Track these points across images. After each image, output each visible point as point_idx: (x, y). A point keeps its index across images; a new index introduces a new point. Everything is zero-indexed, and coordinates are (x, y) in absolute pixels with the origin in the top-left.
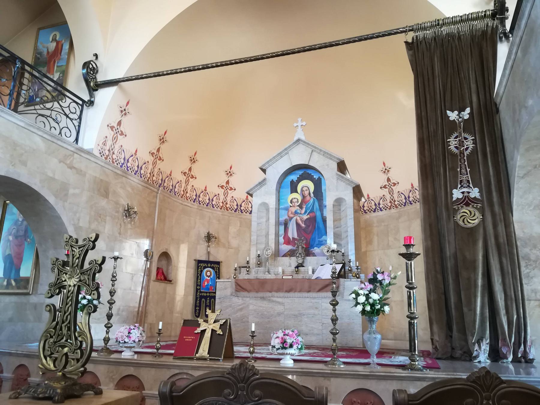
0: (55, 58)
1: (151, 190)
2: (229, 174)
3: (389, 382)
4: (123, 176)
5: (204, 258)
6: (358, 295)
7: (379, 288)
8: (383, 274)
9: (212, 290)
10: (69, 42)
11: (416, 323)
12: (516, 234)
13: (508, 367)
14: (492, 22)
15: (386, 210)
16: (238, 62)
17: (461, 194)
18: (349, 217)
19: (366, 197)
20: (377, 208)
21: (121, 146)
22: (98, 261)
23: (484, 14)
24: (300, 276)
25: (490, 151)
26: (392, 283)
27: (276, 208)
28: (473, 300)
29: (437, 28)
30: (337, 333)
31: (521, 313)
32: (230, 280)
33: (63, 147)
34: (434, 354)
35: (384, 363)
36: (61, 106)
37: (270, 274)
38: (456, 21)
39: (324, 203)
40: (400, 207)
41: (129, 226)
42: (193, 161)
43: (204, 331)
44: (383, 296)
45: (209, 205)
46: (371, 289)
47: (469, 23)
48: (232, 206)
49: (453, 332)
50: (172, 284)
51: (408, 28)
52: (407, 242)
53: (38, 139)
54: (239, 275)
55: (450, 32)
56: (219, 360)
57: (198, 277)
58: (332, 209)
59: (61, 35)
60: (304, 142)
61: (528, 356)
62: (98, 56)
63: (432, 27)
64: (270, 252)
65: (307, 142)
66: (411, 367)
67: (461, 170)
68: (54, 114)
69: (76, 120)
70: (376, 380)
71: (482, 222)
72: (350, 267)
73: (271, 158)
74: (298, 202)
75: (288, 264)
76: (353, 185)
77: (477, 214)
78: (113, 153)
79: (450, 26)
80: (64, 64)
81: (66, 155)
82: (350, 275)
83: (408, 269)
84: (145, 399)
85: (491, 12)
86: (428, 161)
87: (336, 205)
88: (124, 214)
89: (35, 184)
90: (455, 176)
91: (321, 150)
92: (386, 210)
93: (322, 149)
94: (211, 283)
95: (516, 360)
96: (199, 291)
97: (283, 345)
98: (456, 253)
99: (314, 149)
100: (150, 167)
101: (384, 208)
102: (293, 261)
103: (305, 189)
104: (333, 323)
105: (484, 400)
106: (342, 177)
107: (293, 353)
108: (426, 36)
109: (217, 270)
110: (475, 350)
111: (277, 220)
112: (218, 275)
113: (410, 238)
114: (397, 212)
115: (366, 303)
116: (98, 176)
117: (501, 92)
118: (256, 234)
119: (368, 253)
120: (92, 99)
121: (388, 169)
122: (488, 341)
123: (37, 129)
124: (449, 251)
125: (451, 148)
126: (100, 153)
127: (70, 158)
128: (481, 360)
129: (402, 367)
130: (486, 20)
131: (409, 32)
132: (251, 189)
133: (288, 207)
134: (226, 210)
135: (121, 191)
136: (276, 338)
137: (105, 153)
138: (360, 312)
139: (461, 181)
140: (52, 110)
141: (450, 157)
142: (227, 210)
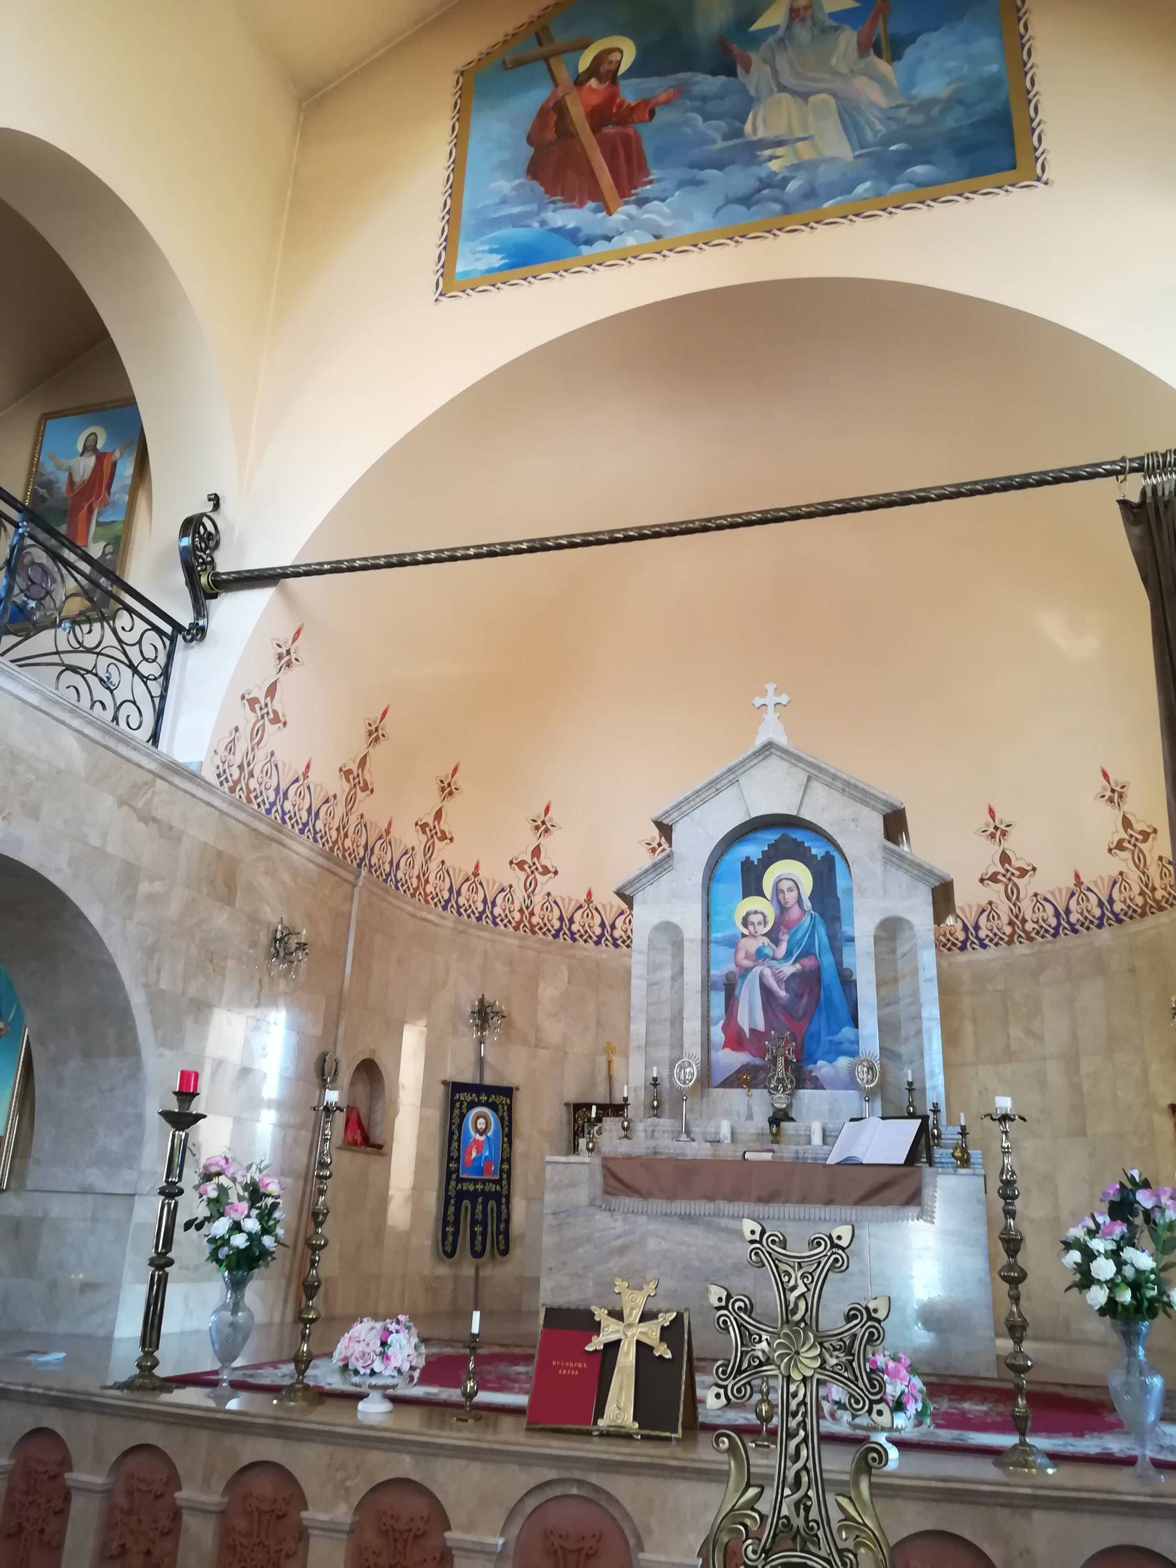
0: (93, 499)
1: (341, 877)
2: (542, 827)
4: (273, 840)
5: (468, 1077)
6: (1089, 1255)
7: (1142, 1232)
9: (490, 1173)
10: (135, 455)
15: (997, 944)
21: (272, 754)
22: (875, 1311)
24: (787, 1151)
33: (129, 760)
36: (120, 641)
37: (694, 1140)
39: (844, 928)
40: (1039, 939)
41: (282, 985)
42: (447, 790)
43: (616, 1344)
46: (1122, 1237)
48: (546, 919)
50: (382, 1155)
53: (69, 741)
56: (669, 1439)
57: (451, 1134)
59: (112, 436)
60: (786, 752)
62: (221, 502)
65: (795, 751)
68: (103, 662)
69: (155, 679)
74: (765, 923)
75: (743, 1110)
76: (932, 881)
78: (251, 775)
80: (120, 517)
81: (135, 785)
84: (452, 1557)
88: (272, 949)
89: (58, 871)
91: (835, 777)
93: (839, 774)
94: (487, 1154)
96: (454, 1176)
99: (815, 772)
100: (340, 810)
103: (785, 885)
107: (900, 1427)
112: (506, 1129)
115: (1119, 1279)
116: (210, 839)
120: (201, 623)
121: (1002, 827)
123: (72, 711)
126: (219, 776)
127: (145, 793)
131: (1129, 473)
132: (630, 883)
133: (735, 935)
134: (530, 933)
135: (264, 882)
137: (231, 775)
139: (1170, 875)
140: (98, 654)
142: (534, 933)
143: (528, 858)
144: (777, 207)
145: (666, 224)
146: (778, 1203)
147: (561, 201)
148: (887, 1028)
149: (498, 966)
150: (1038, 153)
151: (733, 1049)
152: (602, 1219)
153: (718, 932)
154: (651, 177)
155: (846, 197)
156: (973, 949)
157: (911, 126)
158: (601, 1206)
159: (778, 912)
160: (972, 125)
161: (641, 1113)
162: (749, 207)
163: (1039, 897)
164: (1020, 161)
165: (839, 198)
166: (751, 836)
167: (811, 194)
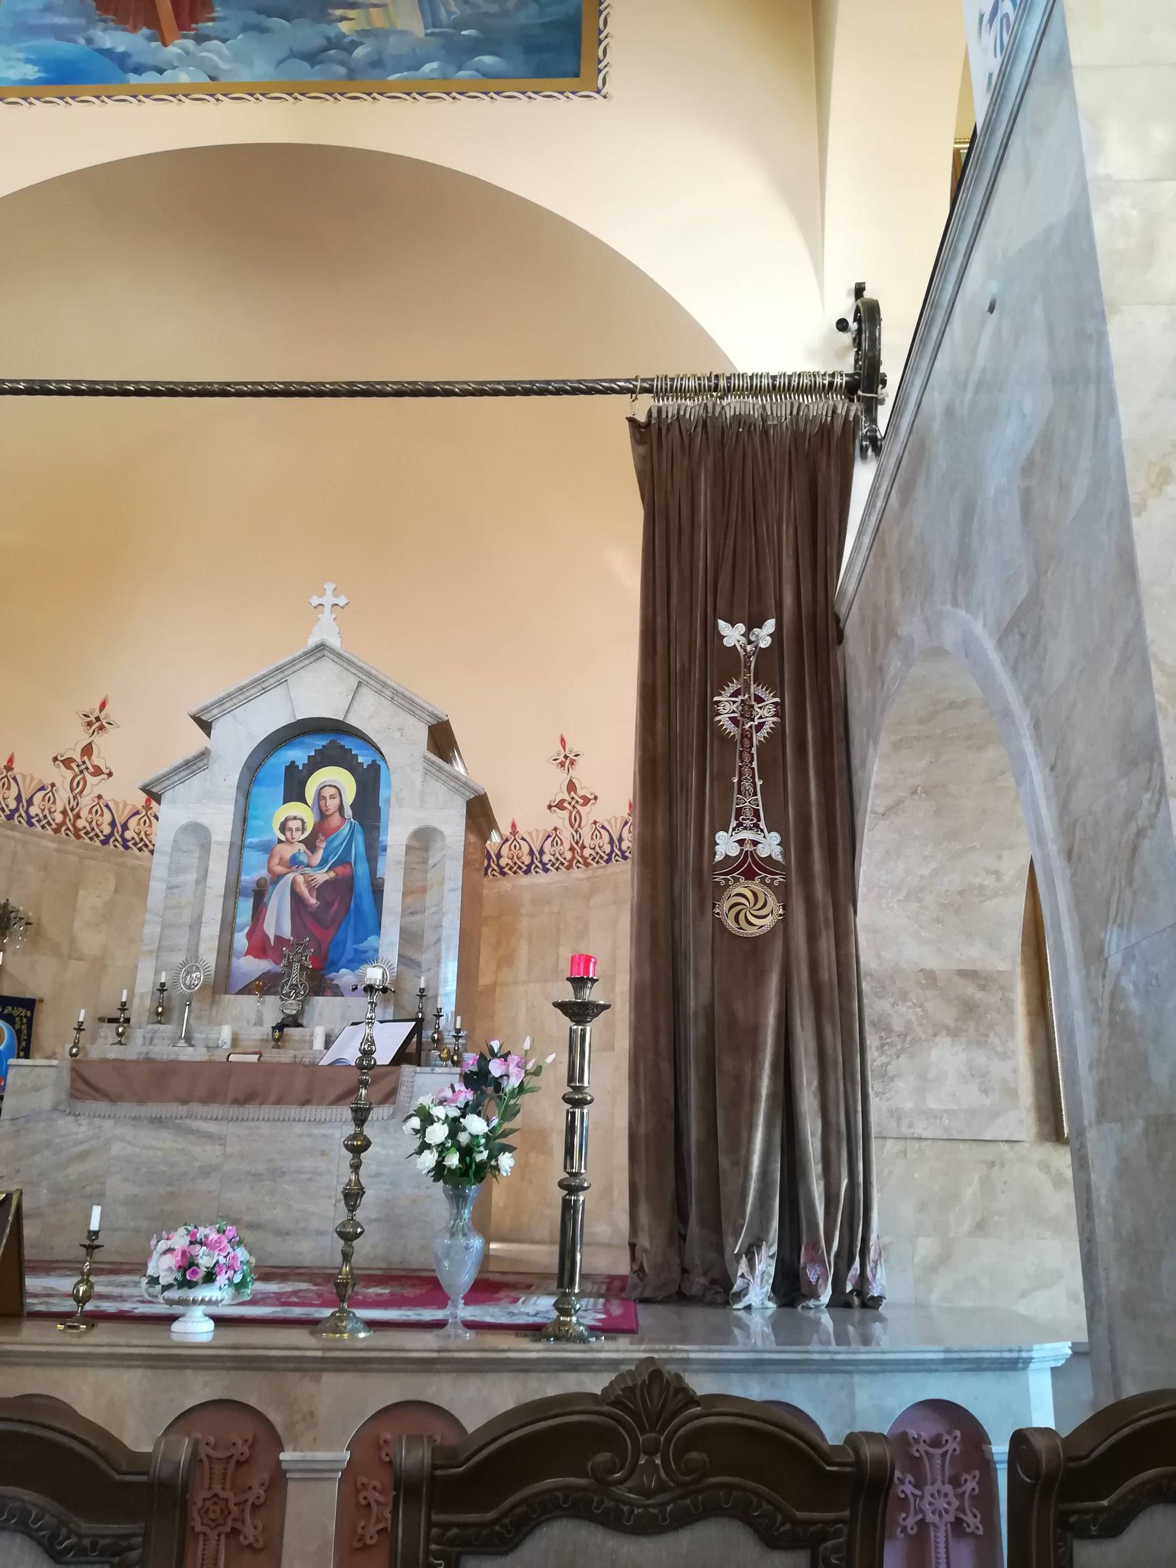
2: (96, 723)
3: (492, 1377)
6: (428, 1119)
8: (506, 1060)
11: (581, 1202)
12: (862, 960)
13: (817, 1322)
14: (846, 405)
15: (557, 869)
16: (99, 389)
17: (737, 844)
18: (448, 885)
19: (506, 830)
20: (536, 863)
23: (829, 382)
24: (284, 1056)
25: (813, 737)
26: (530, 1086)
27: (232, 844)
28: (744, 1136)
29: (712, 396)
30: (358, 1236)
31: (858, 1172)
32: (55, 1062)
34: (635, 1287)
35: (488, 1319)
37: (192, 1046)
38: (761, 386)
40: (595, 865)
44: (500, 1124)
45: (16, 815)
46: (467, 1104)
47: (790, 398)
48: (94, 824)
49: (688, 1224)
51: (638, 384)
52: (579, 969)
54: (88, 1046)
55: (742, 413)
58: (403, 859)
61: (869, 1289)
63: (699, 391)
64: (198, 977)
65: (347, 655)
66: (557, 1331)
67: (740, 781)
70: (455, 1375)
71: (781, 925)
72: (437, 1031)
73: (232, 689)
74: (304, 829)
75: (253, 1017)
76: (467, 793)
77: (772, 902)
79: (744, 398)
82: (436, 1053)
83: (575, 1046)
85: (845, 378)
86: (661, 748)
87: (416, 849)
90: (727, 797)
91: (385, 685)
92: (557, 869)
93: (389, 682)
95: (840, 1302)
97: (184, 1275)
98: (710, 1008)
99: (366, 679)
101: (552, 865)
102: (271, 1009)
103: (328, 792)
104: (347, 1204)
105: (642, 1455)
106: (440, 768)
108: (682, 413)
109: (24, 1027)
110: (739, 1274)
111: (233, 877)
113: (588, 959)
114: (588, 879)
117: (851, 588)
118: (160, 920)
119: (498, 989)
121: (571, 756)
122: (774, 1249)
124: (694, 1000)
125: (720, 721)
128: (753, 1304)
129: (535, 1331)
130: (833, 398)
131: (640, 393)
132: (159, 780)
133: (271, 841)
134: (73, 837)
136: (165, 1252)
138: (429, 1172)
139: (739, 812)
141: (716, 743)
142: (78, 837)
143: (77, 756)
144: (342, 70)
145: (224, 66)
146: (254, 1104)
147: (113, 21)
148: (409, 937)
149: (30, 869)
150: (601, 66)
151: (256, 956)
152: (65, 1124)
153: (253, 837)
154: (214, 15)
155: (412, 74)
156: (537, 872)
157: (486, 14)
158: (65, 1111)
159: (318, 819)
160: (543, 24)
161: (145, 1019)
162: (313, 65)
163: (597, 824)
164: (585, 68)
165: (406, 73)
166: (300, 739)
167: (377, 64)
